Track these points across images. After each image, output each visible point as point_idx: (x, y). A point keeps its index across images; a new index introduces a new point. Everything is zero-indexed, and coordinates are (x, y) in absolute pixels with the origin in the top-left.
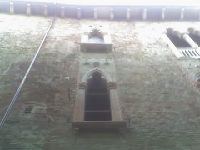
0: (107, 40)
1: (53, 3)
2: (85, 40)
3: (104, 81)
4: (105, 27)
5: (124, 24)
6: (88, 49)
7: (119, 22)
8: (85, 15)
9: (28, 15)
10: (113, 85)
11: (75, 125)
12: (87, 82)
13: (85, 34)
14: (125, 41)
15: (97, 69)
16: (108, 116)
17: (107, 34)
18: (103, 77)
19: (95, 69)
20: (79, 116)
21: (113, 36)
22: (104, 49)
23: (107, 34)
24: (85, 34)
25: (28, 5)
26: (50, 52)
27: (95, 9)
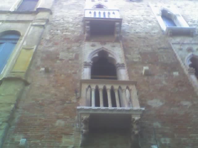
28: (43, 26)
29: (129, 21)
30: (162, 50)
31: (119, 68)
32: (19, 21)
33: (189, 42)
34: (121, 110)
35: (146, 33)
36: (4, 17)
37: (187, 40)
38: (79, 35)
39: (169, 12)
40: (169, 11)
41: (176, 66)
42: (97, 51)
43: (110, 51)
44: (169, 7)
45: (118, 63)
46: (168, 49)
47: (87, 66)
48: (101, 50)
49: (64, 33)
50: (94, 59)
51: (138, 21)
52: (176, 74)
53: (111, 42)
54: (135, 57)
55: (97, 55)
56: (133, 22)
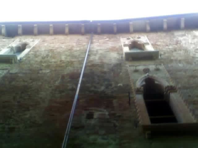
0: (149, 48)
2: (126, 50)
4: (143, 39)
6: (131, 58)
20: (144, 119)
25: (51, 25)
27: (19, 25)
39: (139, 43)
55: (144, 83)
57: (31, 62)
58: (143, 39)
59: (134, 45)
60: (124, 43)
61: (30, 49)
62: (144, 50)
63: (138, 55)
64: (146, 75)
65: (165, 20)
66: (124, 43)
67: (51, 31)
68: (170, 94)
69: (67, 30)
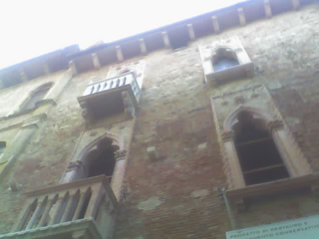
0: (244, 59)
1: (75, 47)
3: (260, 122)
4: (233, 41)
5: (265, 24)
6: (218, 81)
7: (217, 36)
8: (205, 28)
9: (269, 18)
10: (277, 125)
11: (233, 196)
12: (233, 131)
13: (206, 59)
14: (75, 152)
15: (241, 107)
16: (283, 172)
17: (240, 50)
18: (255, 117)
19: (238, 107)
20: (236, 179)
21: (249, 50)
22: (246, 73)
23: (240, 50)
24: (206, 59)
25: (164, 32)
26: (170, 98)
27: (188, 25)
28: (35, 125)
29: (160, 82)
30: (193, 114)
31: (117, 159)
32: (10, 128)
33: (242, 88)
34: (57, 228)
35: (179, 93)
36: (6, 124)
37: (247, 83)
38: (81, 123)
39: (227, 50)
40: (228, 49)
41: (207, 134)
42: (96, 142)
43: (114, 136)
44: (228, 42)
45: (271, 123)
46: (205, 111)
47: (72, 169)
48: (103, 138)
49: (61, 128)
50: (235, 127)
51: (173, 78)
52: (202, 146)
53: (117, 122)
54: (149, 133)
55: (236, 121)
56: (165, 83)
57: (71, 107)
58: (233, 41)
59: (223, 56)
60: (202, 55)
61: (126, 157)
62: (238, 63)
63: (229, 72)
64: (240, 105)
65: (240, 10)
66: (202, 55)
67: (143, 48)
68: (273, 130)
69: (143, 48)
